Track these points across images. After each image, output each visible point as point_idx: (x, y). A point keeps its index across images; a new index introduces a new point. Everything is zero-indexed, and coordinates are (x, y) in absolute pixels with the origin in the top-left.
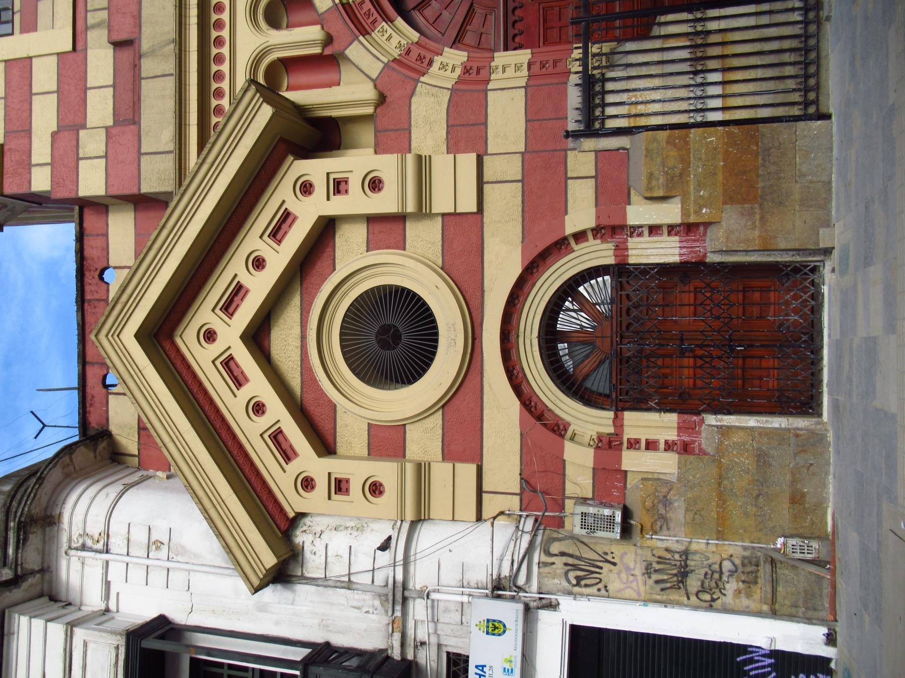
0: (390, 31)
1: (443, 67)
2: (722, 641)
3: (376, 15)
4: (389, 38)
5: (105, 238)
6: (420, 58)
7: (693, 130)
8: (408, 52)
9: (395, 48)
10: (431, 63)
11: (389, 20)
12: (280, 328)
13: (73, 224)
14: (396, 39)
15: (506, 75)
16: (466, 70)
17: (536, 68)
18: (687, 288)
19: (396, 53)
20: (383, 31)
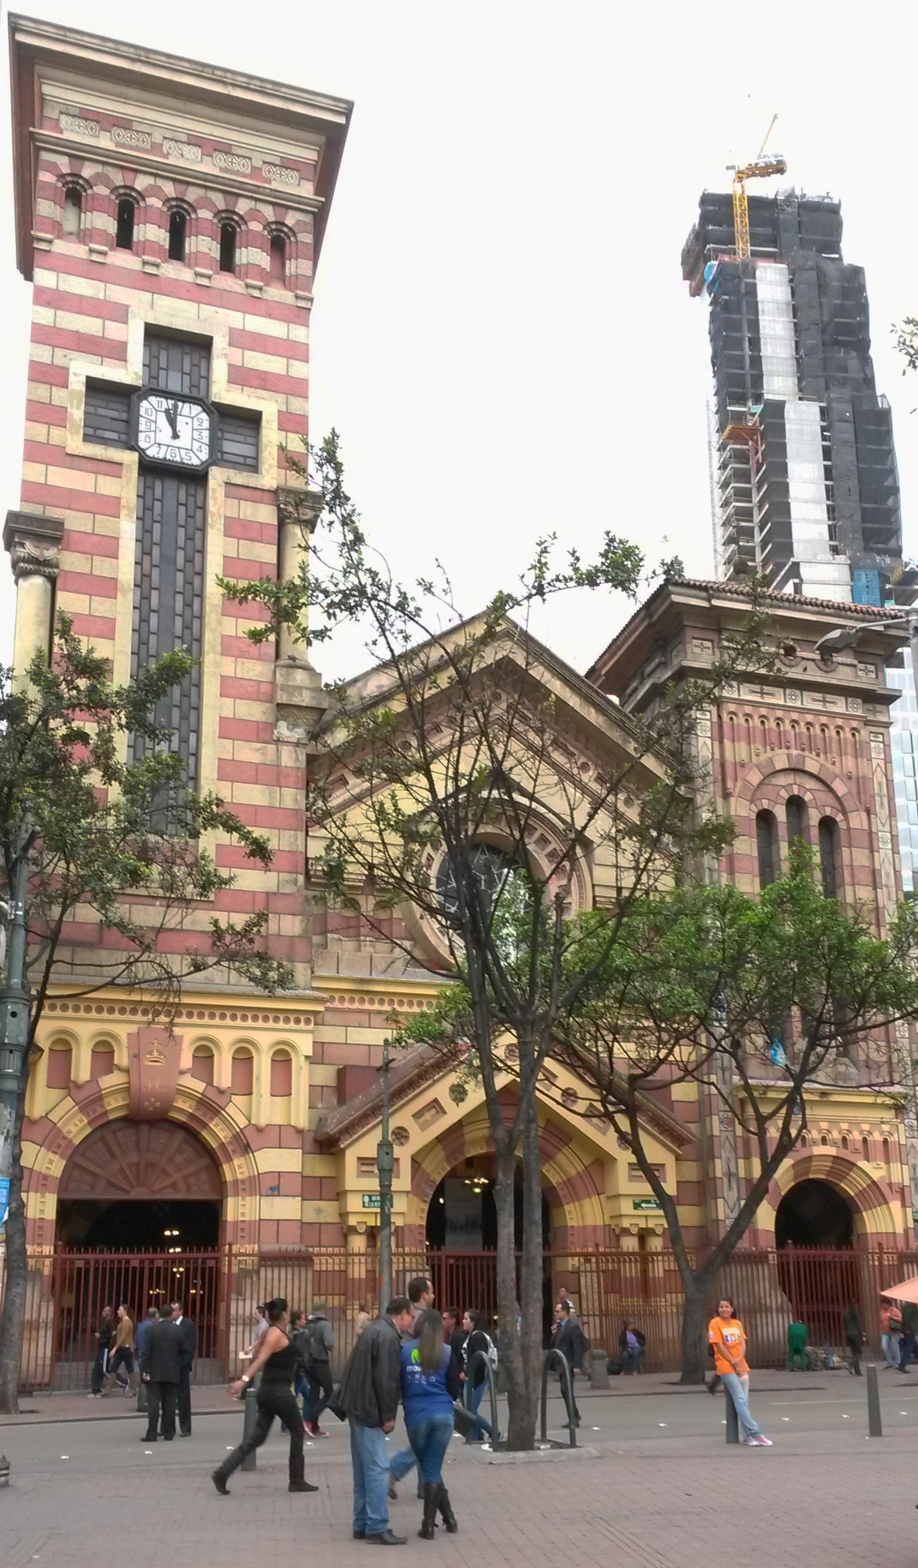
0: (80, 1125)
1: (51, 1162)
2: (707, 350)
3: (93, 1116)
4: (76, 1125)
5: (324, 1180)
6: (59, 1146)
7: (873, 1030)
8: (65, 1138)
9: (364, 1206)
10: (55, 1153)
11: (90, 1123)
12: (43, 1196)
13: (558, 1270)
14: (74, 1130)
15: (38, 1204)
16: (46, 1177)
17: (240, 1226)
18: (414, 1275)
19: (65, 1131)
20: (81, 1121)
